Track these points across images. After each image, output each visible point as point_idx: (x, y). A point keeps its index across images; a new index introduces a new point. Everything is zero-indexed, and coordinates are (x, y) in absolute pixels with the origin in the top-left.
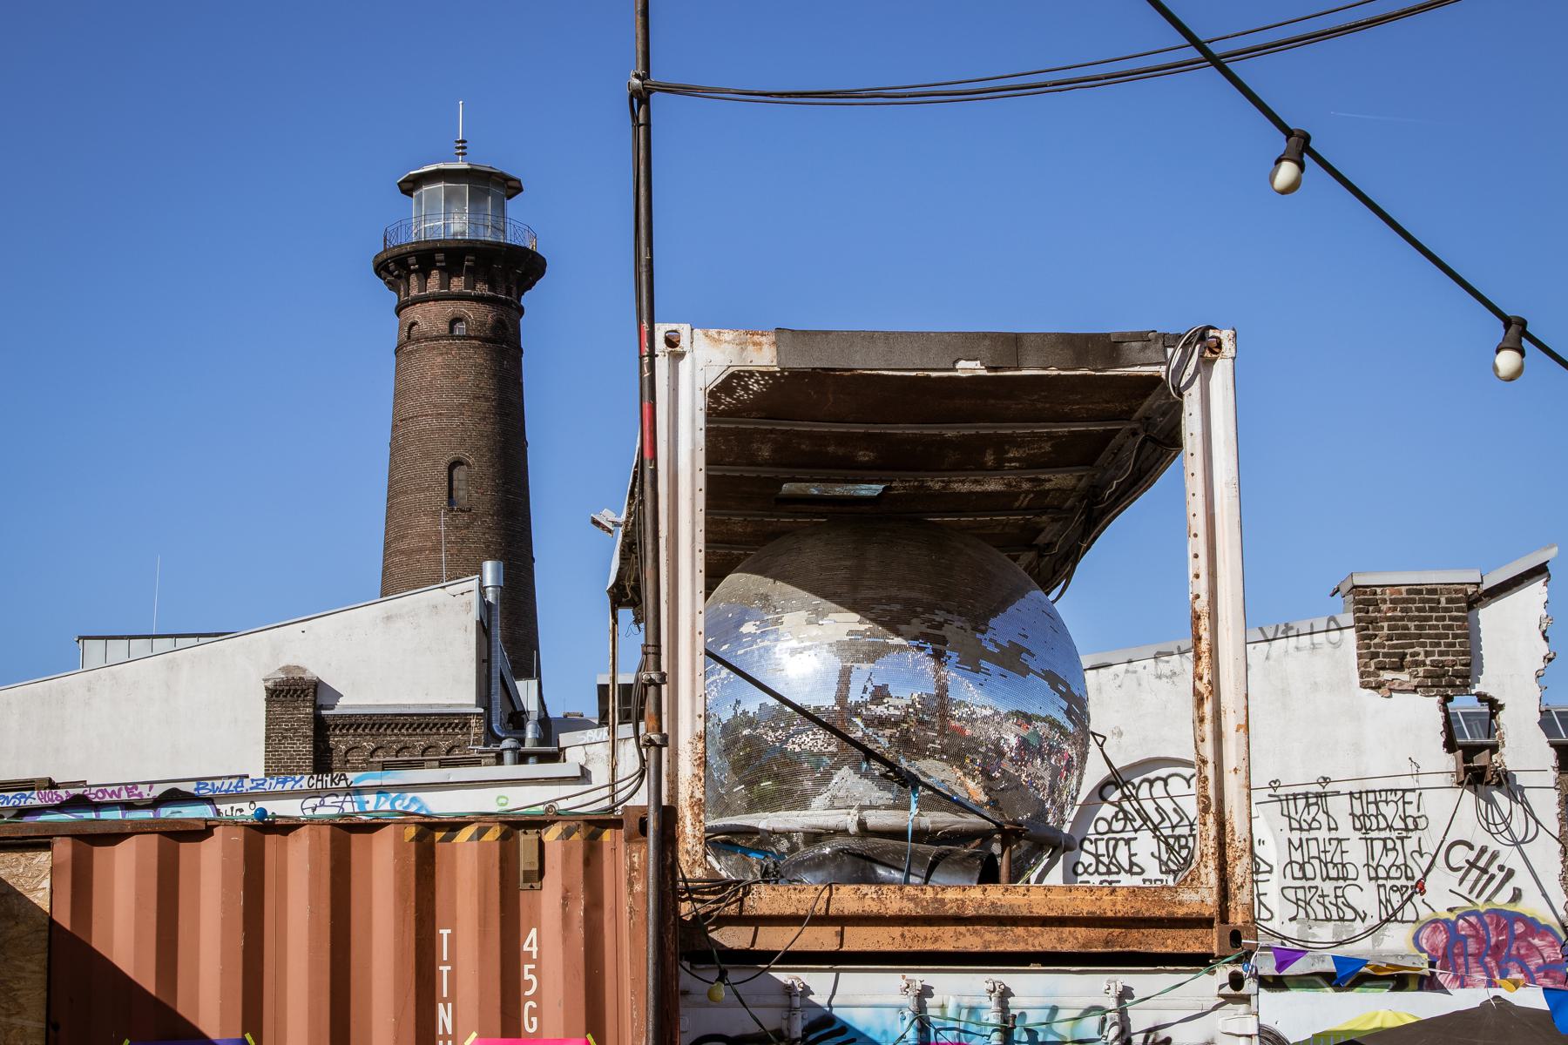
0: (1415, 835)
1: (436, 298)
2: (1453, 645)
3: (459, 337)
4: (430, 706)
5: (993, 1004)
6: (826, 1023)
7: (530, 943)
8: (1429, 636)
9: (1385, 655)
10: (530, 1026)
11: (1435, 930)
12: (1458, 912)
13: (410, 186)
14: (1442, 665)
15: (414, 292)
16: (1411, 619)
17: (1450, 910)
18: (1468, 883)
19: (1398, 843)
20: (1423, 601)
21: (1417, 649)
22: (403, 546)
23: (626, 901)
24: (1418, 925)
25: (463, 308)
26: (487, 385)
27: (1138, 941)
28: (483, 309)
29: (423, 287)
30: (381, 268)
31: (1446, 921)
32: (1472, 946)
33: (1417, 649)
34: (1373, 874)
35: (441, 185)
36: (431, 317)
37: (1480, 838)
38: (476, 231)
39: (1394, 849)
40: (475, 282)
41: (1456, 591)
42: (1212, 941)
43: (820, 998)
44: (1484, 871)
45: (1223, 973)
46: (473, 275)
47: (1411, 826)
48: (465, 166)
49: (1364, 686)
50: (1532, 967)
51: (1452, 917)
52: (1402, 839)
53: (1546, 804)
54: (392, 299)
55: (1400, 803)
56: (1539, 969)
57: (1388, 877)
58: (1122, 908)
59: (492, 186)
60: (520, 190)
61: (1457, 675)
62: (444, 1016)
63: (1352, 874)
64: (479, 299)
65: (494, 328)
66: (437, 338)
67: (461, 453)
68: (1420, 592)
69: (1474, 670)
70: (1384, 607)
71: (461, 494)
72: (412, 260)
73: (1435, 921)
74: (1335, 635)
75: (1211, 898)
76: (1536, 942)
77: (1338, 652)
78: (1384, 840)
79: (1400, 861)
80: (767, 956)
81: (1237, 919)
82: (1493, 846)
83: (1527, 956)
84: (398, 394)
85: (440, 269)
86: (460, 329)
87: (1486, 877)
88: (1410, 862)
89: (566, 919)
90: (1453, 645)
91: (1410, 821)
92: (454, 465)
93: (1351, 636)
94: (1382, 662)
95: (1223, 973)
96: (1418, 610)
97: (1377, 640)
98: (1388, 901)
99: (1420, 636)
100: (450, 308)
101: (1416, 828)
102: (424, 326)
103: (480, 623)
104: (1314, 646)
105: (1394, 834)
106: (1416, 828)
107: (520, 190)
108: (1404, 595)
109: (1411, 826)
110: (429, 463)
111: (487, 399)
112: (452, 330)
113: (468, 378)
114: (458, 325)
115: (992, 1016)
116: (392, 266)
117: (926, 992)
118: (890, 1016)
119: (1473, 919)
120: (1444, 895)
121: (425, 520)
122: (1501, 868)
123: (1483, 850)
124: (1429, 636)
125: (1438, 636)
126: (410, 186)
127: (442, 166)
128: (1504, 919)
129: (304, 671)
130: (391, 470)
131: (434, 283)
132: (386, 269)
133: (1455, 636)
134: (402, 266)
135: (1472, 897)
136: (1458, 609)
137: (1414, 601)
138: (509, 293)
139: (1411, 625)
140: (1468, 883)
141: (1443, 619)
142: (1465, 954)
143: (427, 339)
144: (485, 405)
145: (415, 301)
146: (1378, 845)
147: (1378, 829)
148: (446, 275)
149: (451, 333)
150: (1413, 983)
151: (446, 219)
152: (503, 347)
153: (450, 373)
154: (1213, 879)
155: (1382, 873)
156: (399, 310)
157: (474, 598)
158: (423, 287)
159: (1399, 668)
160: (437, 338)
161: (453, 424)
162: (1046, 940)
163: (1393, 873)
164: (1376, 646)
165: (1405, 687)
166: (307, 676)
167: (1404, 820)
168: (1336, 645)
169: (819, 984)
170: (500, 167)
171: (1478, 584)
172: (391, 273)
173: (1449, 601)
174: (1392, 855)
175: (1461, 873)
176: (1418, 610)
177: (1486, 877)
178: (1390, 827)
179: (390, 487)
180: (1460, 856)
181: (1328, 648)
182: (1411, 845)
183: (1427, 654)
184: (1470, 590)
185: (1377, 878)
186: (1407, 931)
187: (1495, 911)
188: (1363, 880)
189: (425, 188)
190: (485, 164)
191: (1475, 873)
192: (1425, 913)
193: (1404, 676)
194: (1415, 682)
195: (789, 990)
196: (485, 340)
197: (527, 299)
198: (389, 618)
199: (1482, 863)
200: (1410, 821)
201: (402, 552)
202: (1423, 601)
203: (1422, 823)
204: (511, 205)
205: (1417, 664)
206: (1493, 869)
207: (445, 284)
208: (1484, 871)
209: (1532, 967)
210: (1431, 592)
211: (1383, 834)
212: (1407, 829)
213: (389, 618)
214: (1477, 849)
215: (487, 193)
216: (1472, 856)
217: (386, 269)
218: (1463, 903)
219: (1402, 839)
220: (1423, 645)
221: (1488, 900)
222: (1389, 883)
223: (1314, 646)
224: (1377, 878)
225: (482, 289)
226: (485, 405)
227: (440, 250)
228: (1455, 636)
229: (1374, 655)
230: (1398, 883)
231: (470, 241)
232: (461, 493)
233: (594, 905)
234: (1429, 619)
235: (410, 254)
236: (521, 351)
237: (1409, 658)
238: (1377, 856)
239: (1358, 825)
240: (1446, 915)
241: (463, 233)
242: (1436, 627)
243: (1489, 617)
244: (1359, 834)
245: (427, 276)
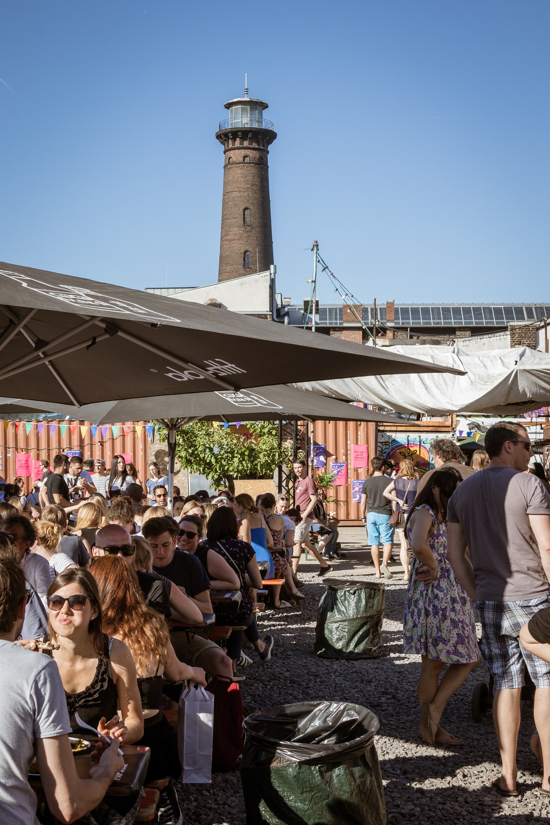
1: (239, 148)
3: (247, 163)
4: (255, 312)
5: (418, 438)
6: (394, 441)
7: (359, 433)
10: (359, 443)
13: (229, 106)
15: (230, 146)
22: (228, 238)
23: (371, 428)
25: (248, 152)
26: (257, 181)
27: (439, 429)
28: (255, 152)
29: (234, 144)
30: (218, 137)
35: (240, 106)
36: (237, 155)
38: (251, 124)
40: (252, 142)
42: (450, 429)
43: (393, 437)
45: (451, 434)
46: (252, 140)
48: (248, 99)
54: (222, 148)
58: (437, 425)
59: (258, 106)
60: (267, 107)
61: (533, 346)
62: (349, 442)
64: (254, 149)
65: (259, 159)
66: (239, 163)
67: (248, 205)
71: (248, 220)
72: (230, 134)
74: (505, 336)
75: (450, 423)
80: (387, 431)
81: (454, 426)
84: (225, 183)
85: (240, 138)
86: (247, 160)
89: (364, 430)
92: (245, 209)
93: (509, 337)
95: (451, 434)
100: (243, 152)
102: (234, 159)
103: (270, 286)
104: (500, 339)
107: (267, 107)
110: (237, 209)
111: (257, 186)
112: (244, 160)
114: (246, 158)
115: (418, 440)
116: (223, 136)
117: (409, 436)
118: (404, 439)
121: (235, 229)
126: (229, 106)
127: (240, 99)
129: (216, 300)
130: (223, 211)
131: (237, 143)
132: (221, 137)
134: (225, 136)
138: (264, 146)
143: (235, 163)
144: (256, 188)
148: (242, 140)
149: (244, 162)
151: (242, 120)
152: (262, 165)
153: (243, 176)
154: (451, 420)
157: (268, 277)
158: (234, 144)
160: (239, 163)
161: (243, 195)
162: (426, 429)
166: (217, 302)
168: (505, 339)
169: (394, 435)
170: (264, 101)
172: (222, 139)
179: (223, 217)
181: (503, 340)
189: (234, 107)
190: (255, 99)
195: (389, 436)
196: (256, 164)
197: (270, 148)
198: (242, 284)
201: (228, 240)
204: (264, 112)
205: (524, 344)
207: (241, 143)
213: (242, 284)
217: (221, 137)
223: (500, 339)
225: (255, 145)
226: (256, 188)
227: (240, 131)
229: (514, 342)
231: (250, 128)
232: (248, 219)
233: (367, 429)
235: (229, 132)
236: (268, 167)
241: (247, 124)
245: (235, 140)
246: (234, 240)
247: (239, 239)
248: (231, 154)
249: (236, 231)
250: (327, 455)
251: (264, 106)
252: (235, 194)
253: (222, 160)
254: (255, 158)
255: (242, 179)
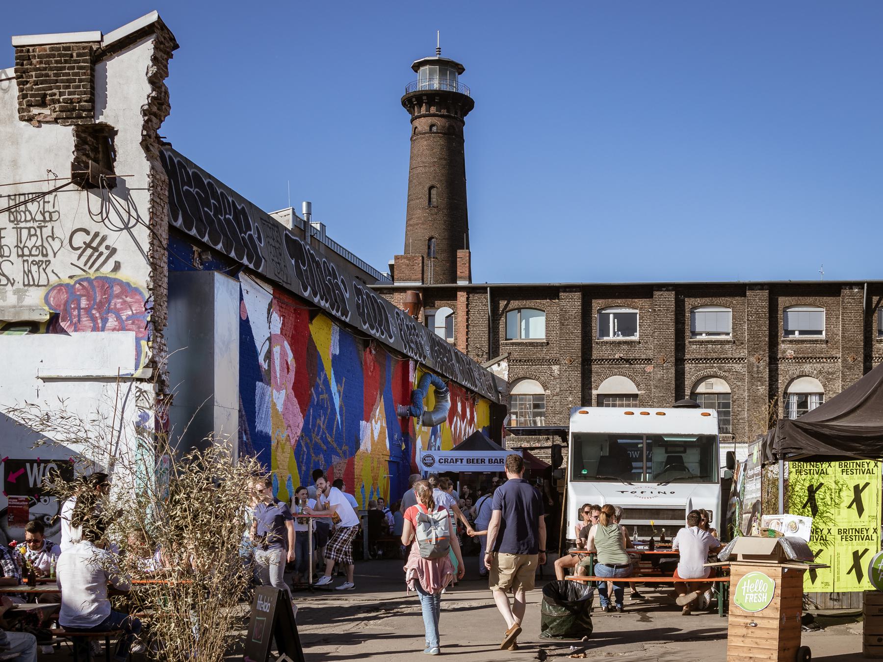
0: (49, 225)
1: (424, 116)
2: (79, 87)
3: (434, 133)
8: (62, 81)
9: (32, 96)
11: (60, 290)
12: (75, 279)
14: (71, 101)
15: (416, 114)
16: (51, 69)
17: (71, 277)
18: (84, 259)
19: (38, 230)
20: (60, 55)
21: (54, 91)
24: (49, 288)
25: (435, 120)
28: (443, 120)
31: (68, 285)
32: (84, 303)
33: (54, 91)
34: (20, 253)
36: (423, 124)
37: (94, 228)
39: (35, 235)
41: (84, 48)
44: (95, 249)
46: (440, 106)
47: (48, 219)
49: (22, 119)
50: (124, 317)
51: (72, 282)
52: (41, 228)
53: (143, 200)
55: (41, 203)
56: (128, 318)
57: (31, 255)
60: (464, 70)
63: (7, 253)
64: (442, 116)
65: (448, 129)
68: (58, 49)
69: (98, 106)
70: (34, 61)
71: (434, 200)
72: (414, 100)
73: (60, 285)
76: (128, 299)
77: (7, 96)
78: (29, 229)
79: (39, 243)
82: (104, 231)
83: (122, 309)
84: (411, 158)
86: (434, 129)
87: (96, 254)
88: (46, 244)
90: (79, 87)
91: (47, 215)
92: (431, 188)
94: (33, 102)
96: (57, 62)
97: (28, 85)
98: (30, 271)
99: (57, 81)
100: (430, 120)
101: (51, 220)
105: (36, 225)
106: (51, 220)
108: (48, 52)
109: (48, 219)
111: (445, 159)
112: (431, 129)
113: (437, 150)
119: (85, 284)
120: (65, 266)
121: (419, 211)
122: (107, 247)
123: (97, 235)
124: (62, 81)
125: (68, 81)
126: (416, 67)
128: (106, 283)
131: (423, 110)
133: (80, 81)
134: (413, 102)
135: (86, 268)
136: (84, 61)
137: (54, 56)
138: (456, 113)
139: (51, 73)
140: (84, 259)
141: (73, 68)
142: (79, 308)
143: (421, 134)
145: (419, 117)
146: (25, 233)
147: (26, 221)
150: (42, 329)
151: (429, 81)
153: (429, 150)
155: (26, 252)
156: (412, 121)
159: (43, 104)
163: (34, 252)
164: (27, 89)
165: (48, 119)
167: (43, 215)
171: (99, 42)
173: (78, 55)
174: (34, 239)
175: (81, 250)
176: (57, 62)
177: (96, 254)
178: (33, 219)
180: (80, 240)
182: (47, 232)
183: (61, 94)
184: (95, 47)
185: (23, 255)
186: (42, 292)
187: (101, 277)
188: (14, 257)
190: (445, 56)
191: (89, 251)
192: (53, 279)
193: (46, 111)
194: (54, 115)
199: (94, 245)
200: (47, 215)
202: (60, 55)
203: (55, 216)
204: (460, 78)
205: (54, 102)
206: (102, 248)
207: (428, 110)
208: (95, 249)
209: (124, 317)
210: (65, 49)
211: (28, 225)
212: (44, 221)
214: (92, 234)
215: (447, 70)
216: (88, 239)
218: (79, 272)
219: (41, 228)
220: (58, 88)
221: (97, 270)
222: (31, 259)
224: (23, 255)
225: (444, 112)
226: (444, 162)
227: (425, 95)
228: (80, 81)
230: (37, 259)
234: (64, 68)
237: (48, 98)
238: (23, 242)
239: (12, 219)
240: (67, 281)
242: (68, 74)
243: (114, 67)
244: (12, 225)
245: (421, 106)
246: (417, 224)
247: (423, 224)
248: (417, 123)
249: (420, 214)
250: (45, 95)
251: (460, 69)
252: (419, 170)
253: (410, 128)
254: (444, 127)
255: (428, 152)
